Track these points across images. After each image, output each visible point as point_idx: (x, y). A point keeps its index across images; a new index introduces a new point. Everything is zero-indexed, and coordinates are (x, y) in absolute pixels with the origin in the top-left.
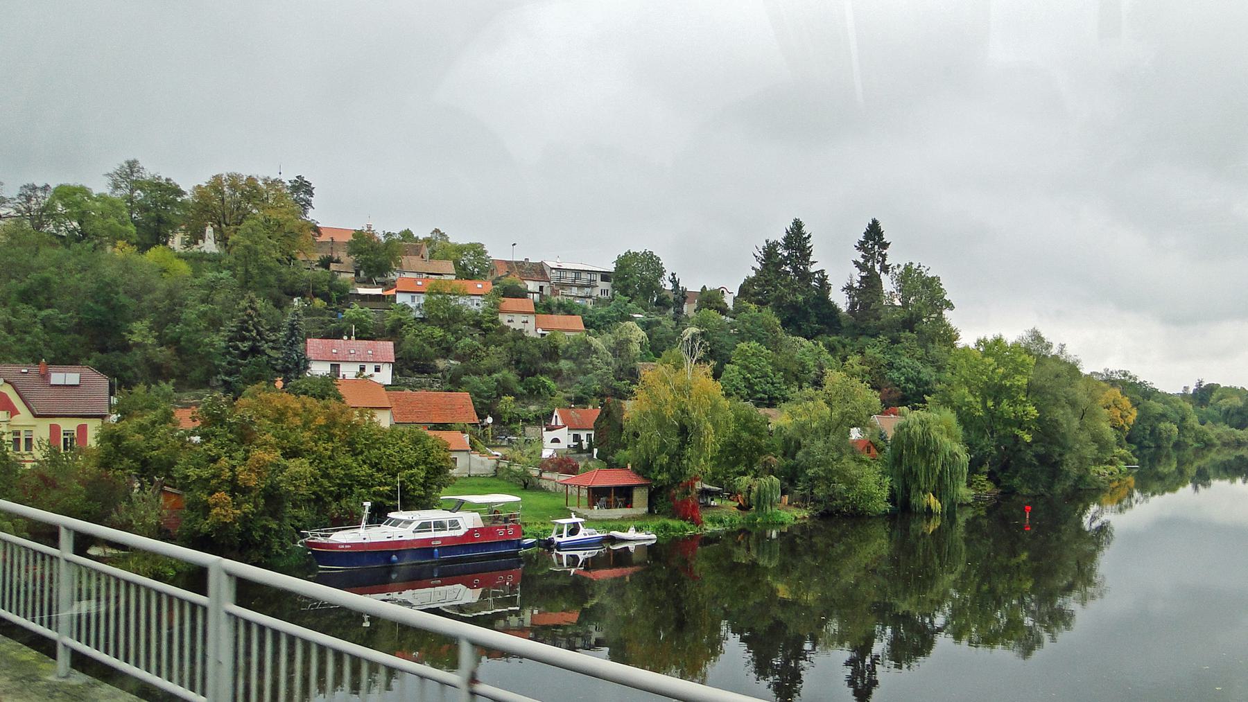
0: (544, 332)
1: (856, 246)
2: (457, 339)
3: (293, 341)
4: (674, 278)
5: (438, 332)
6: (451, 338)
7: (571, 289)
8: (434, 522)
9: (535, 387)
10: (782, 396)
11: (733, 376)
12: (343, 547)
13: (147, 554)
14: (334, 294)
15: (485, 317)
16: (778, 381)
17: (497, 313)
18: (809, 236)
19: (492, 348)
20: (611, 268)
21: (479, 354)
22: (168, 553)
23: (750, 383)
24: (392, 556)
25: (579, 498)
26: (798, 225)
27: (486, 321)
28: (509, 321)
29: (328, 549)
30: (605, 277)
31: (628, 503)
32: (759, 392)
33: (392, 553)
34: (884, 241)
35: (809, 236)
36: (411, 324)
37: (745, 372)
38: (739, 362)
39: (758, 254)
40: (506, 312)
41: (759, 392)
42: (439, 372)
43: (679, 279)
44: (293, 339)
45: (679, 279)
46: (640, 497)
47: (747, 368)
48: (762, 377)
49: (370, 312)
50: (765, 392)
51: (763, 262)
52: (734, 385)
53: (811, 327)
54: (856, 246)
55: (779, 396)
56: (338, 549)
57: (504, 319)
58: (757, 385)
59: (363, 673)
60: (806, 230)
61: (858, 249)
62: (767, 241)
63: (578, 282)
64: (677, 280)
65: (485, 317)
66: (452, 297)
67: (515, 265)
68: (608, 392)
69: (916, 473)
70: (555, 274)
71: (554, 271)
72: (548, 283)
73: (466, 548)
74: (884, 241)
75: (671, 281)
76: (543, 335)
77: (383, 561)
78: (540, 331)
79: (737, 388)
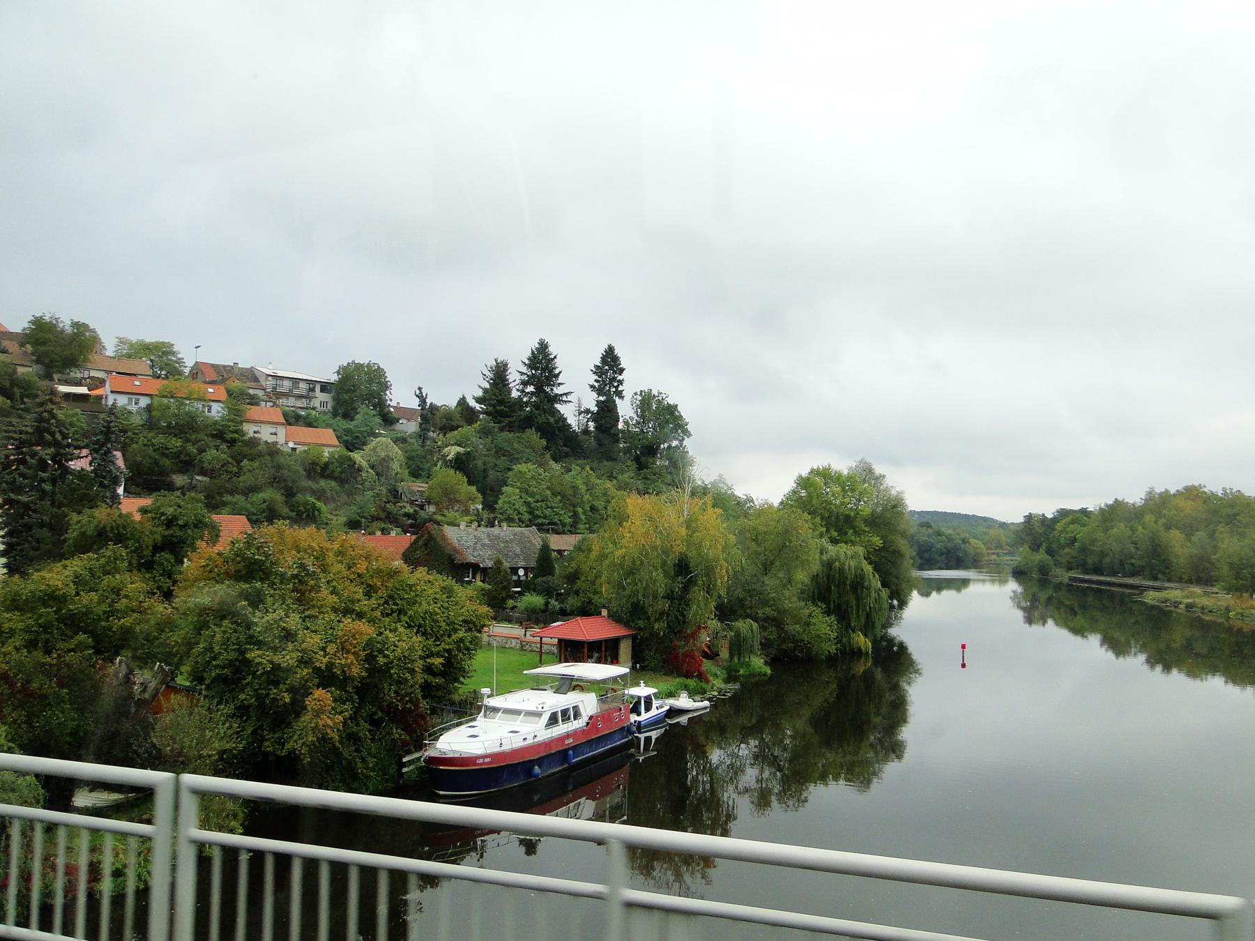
0: (296, 446)
1: (592, 371)
2: (201, 451)
3: (108, 449)
4: (421, 393)
5: (176, 443)
6: (192, 449)
7: (288, 399)
8: (573, 707)
9: (305, 509)
10: (561, 521)
11: (514, 500)
12: (481, 761)
13: (324, 812)
14: (17, 391)
15: (230, 427)
16: (556, 505)
17: (241, 423)
18: (555, 357)
19: (245, 462)
20: (334, 378)
21: (229, 470)
22: (216, 790)
23: (530, 508)
24: (534, 766)
25: (541, 656)
26: (543, 347)
27: (230, 431)
28: (255, 432)
29: (462, 766)
30: (325, 387)
31: (615, 661)
32: (540, 517)
33: (532, 763)
34: (621, 366)
35: (555, 357)
36: (137, 431)
37: (524, 495)
38: (518, 484)
39: (488, 373)
40: (254, 422)
41: (540, 517)
42: (178, 489)
43: (427, 394)
44: (109, 446)
45: (427, 394)
46: (625, 649)
47: (527, 492)
48: (542, 501)
49: (82, 414)
50: (545, 517)
51: (491, 381)
52: (515, 510)
53: (559, 450)
54: (592, 371)
55: (558, 522)
56: (475, 764)
57: (249, 429)
58: (537, 510)
59: (108, 915)
60: (553, 350)
61: (594, 373)
62: (496, 360)
63: (296, 392)
64: (424, 395)
65: (230, 427)
66: (188, 402)
67: (222, 369)
68: (383, 515)
69: (846, 611)
70: (271, 382)
71: (270, 378)
72: (263, 391)
73: (592, 743)
74: (621, 366)
75: (417, 396)
76: (294, 449)
77: (522, 777)
78: (291, 445)
79: (519, 513)
